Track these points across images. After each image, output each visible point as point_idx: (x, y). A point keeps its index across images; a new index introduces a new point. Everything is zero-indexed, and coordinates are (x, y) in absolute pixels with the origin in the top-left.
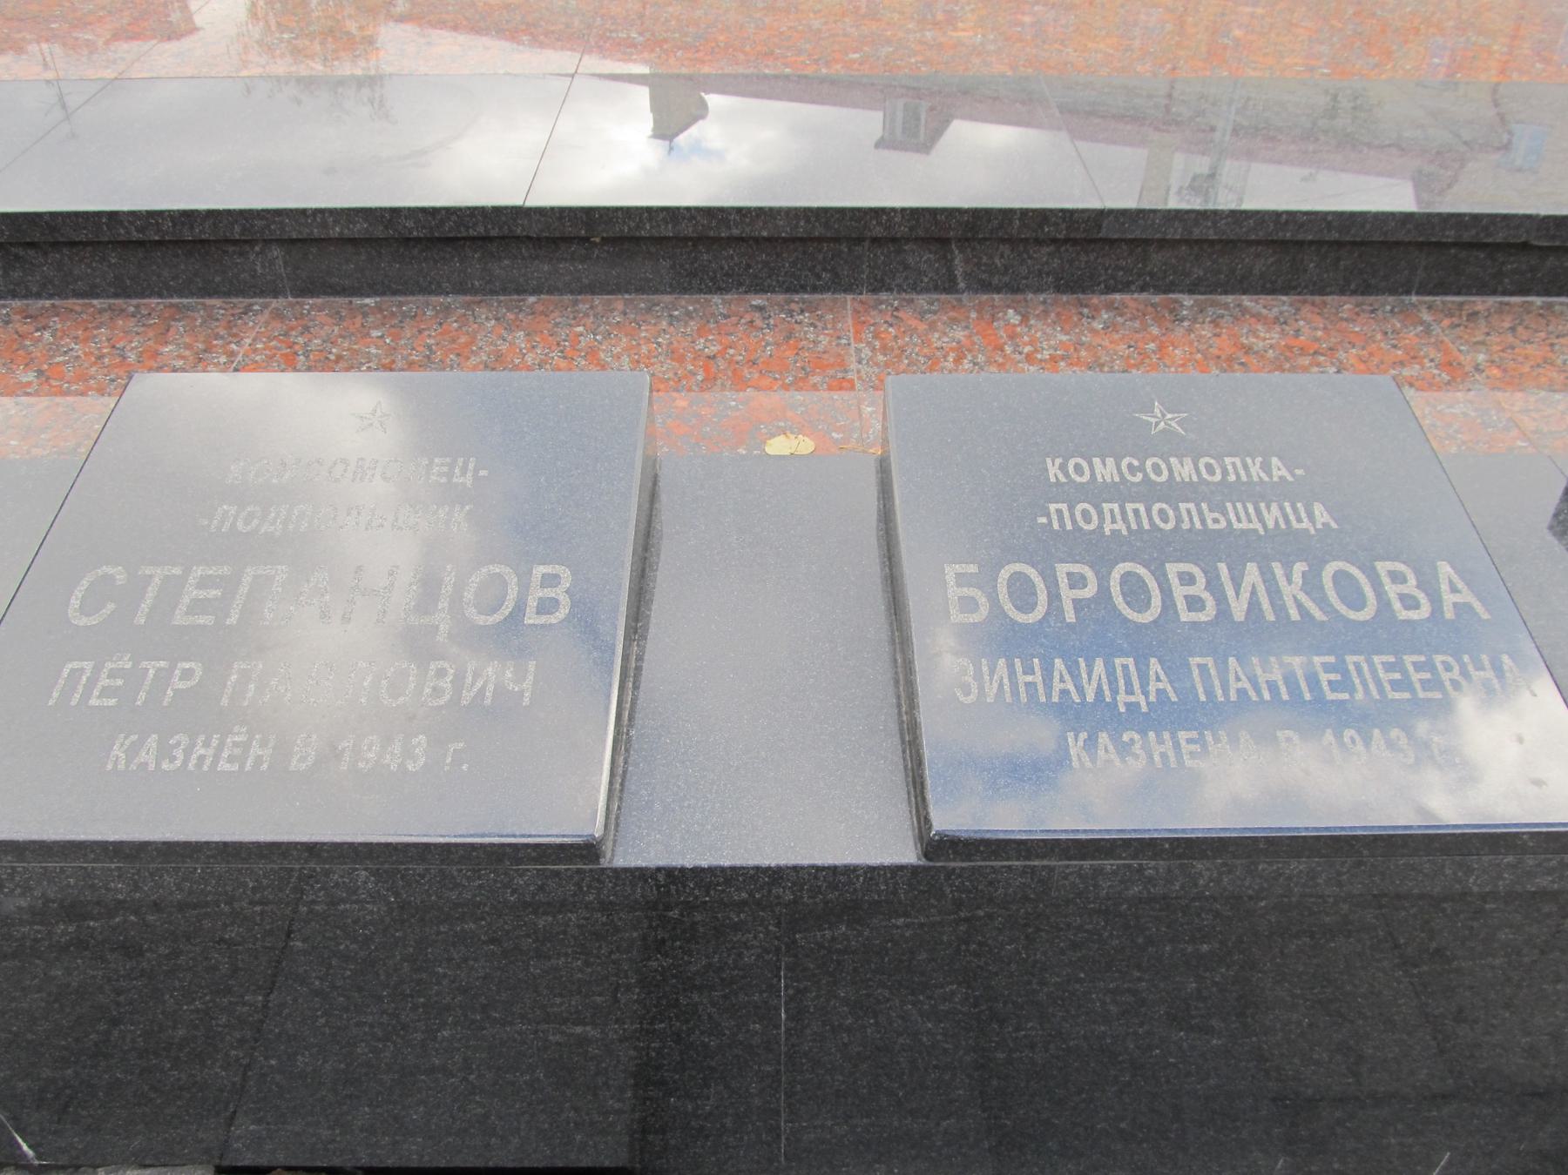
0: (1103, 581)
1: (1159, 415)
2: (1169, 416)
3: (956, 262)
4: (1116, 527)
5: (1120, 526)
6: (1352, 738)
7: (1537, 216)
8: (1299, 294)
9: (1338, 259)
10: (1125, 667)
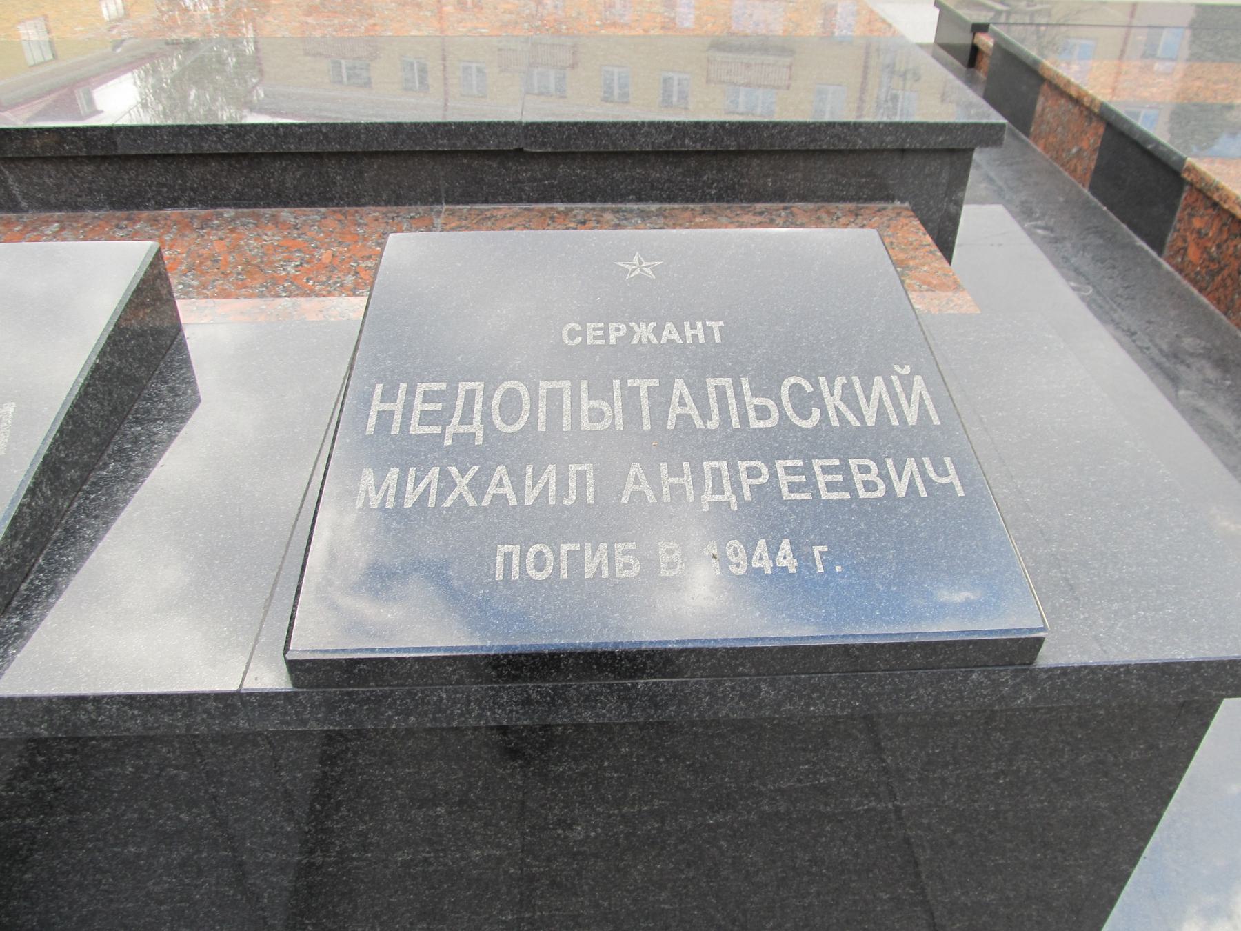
1: (645, 269)
3: (10, 182)
6: (735, 549)
7: (520, 123)
8: (337, 205)
9: (361, 173)
10: (581, 475)
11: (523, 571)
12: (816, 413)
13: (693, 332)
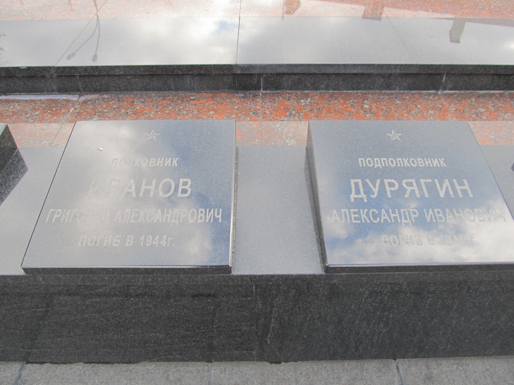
0: (400, 184)
2: (397, 135)
4: (378, 166)
5: (379, 165)
11: (389, 164)
12: (378, 219)
13: (149, 187)
